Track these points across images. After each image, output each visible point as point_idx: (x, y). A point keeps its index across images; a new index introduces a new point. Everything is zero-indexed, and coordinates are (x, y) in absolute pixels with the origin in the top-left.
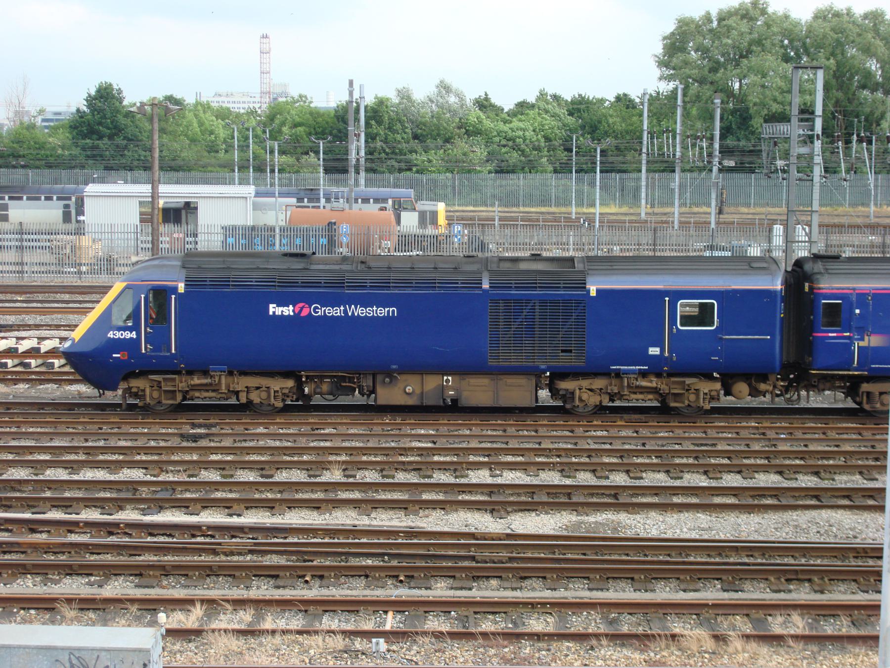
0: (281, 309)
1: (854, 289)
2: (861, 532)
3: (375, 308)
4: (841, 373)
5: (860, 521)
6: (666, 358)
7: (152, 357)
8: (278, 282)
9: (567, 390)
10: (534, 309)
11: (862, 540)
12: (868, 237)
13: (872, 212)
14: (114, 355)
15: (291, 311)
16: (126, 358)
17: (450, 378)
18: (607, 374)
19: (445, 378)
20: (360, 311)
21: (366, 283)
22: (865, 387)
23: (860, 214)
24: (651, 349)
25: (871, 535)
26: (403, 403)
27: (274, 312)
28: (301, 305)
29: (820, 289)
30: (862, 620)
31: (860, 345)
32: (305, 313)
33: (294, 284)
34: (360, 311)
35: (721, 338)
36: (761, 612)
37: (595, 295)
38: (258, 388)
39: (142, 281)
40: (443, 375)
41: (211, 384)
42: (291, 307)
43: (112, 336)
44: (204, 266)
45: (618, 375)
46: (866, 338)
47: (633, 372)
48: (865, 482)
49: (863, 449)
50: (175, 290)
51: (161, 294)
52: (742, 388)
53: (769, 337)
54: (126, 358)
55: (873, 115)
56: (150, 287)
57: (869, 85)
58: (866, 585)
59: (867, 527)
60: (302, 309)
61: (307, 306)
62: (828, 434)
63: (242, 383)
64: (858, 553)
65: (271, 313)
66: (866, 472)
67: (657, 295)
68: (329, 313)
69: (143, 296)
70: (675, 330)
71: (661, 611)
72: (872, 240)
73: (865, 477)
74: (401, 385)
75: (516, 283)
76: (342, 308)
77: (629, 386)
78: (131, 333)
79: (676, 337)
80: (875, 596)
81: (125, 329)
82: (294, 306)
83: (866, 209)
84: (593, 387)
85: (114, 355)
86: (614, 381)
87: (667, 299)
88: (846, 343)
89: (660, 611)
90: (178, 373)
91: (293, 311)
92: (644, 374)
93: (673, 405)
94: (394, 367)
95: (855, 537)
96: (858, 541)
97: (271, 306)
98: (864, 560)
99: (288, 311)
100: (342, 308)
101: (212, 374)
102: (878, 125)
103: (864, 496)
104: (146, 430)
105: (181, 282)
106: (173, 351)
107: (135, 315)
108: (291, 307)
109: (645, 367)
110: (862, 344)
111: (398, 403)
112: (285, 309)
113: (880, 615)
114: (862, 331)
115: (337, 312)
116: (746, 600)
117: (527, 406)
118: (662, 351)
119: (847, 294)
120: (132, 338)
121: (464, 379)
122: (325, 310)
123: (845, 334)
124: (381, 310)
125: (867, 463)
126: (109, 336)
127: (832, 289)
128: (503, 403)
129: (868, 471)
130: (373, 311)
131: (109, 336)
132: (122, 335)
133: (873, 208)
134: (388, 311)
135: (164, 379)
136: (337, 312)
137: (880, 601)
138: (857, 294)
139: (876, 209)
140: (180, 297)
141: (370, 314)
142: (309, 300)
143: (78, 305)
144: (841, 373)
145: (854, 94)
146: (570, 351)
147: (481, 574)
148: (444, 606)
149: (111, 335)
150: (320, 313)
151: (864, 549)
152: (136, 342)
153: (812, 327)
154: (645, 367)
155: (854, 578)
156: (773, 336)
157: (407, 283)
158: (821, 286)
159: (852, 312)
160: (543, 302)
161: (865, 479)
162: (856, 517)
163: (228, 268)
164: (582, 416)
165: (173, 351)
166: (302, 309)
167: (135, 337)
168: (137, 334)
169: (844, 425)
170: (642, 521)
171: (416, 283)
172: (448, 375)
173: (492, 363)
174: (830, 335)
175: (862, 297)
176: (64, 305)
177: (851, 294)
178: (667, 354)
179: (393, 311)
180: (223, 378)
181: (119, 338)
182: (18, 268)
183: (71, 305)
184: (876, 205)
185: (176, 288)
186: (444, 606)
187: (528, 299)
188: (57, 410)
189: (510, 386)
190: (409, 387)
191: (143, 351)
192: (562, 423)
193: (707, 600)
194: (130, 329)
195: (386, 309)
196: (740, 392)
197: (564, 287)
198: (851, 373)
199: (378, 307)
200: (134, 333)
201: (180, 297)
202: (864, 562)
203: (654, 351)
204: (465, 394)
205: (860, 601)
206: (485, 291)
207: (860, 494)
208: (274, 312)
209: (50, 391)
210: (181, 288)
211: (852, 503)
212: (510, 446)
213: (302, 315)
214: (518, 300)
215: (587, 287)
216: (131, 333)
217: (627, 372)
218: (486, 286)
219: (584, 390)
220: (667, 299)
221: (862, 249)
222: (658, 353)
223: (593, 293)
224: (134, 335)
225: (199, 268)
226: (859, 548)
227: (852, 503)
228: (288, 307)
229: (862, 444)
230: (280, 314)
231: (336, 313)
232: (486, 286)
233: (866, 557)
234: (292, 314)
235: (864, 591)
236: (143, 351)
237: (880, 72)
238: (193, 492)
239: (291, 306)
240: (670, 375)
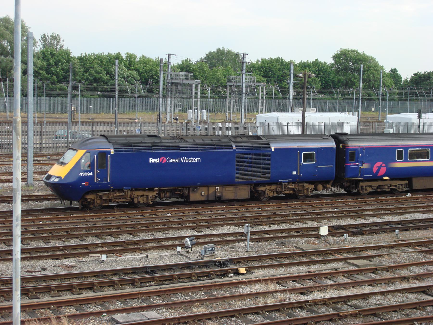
0: (154, 160)
2: (5, 272)
3: (192, 159)
5: (4, 266)
6: (298, 176)
9: (262, 191)
11: (6, 275)
12: (6, 127)
13: (8, 115)
14: (82, 184)
16: (87, 185)
18: (276, 183)
19: (217, 188)
20: (186, 160)
21: (122, 148)
22: (361, 184)
23: (2, 116)
24: (293, 172)
25: (10, 273)
26: (200, 200)
27: (151, 162)
28: (162, 158)
29: (348, 146)
30: (7, 315)
32: (164, 162)
33: (159, 149)
34: (186, 160)
35: (317, 167)
36: (31, 308)
38: (141, 196)
39: (94, 149)
40: (216, 187)
42: (158, 159)
43: (81, 175)
44: (118, 142)
45: (281, 183)
46: (363, 165)
48: (7, 247)
49: (5, 231)
50: (109, 153)
51: (103, 155)
52: (320, 186)
55: (7, 67)
56: (98, 152)
57: (4, 53)
58: (8, 297)
59: (8, 269)
60: (163, 159)
62: (35, 222)
64: (4, 282)
65: (150, 162)
66: (7, 242)
67: (295, 150)
69: (96, 156)
71: (31, 309)
72: (8, 129)
73: (7, 245)
76: (179, 159)
77: (285, 188)
78: (90, 173)
79: (302, 166)
80: (8, 303)
81: (87, 171)
82: (160, 159)
83: (5, 114)
84: (272, 189)
85: (82, 184)
86: (279, 186)
87: (299, 152)
89: (78, 303)
90: (109, 191)
91: (159, 161)
92: (289, 183)
94: (199, 184)
95: (2, 275)
96: (4, 276)
97: (150, 159)
98: (7, 285)
99: (157, 161)
100: (179, 159)
102: (10, 72)
103: (6, 254)
104: (41, 223)
105: (112, 149)
106: (109, 181)
107: (91, 166)
108: (158, 159)
110: (362, 167)
111: (198, 200)
112: (156, 160)
113: (12, 312)
114: (362, 163)
115: (177, 160)
116: (124, 293)
118: (297, 173)
120: (90, 176)
121: (224, 188)
125: (8, 238)
126: (80, 175)
128: (239, 197)
129: (8, 242)
131: (80, 175)
132: (86, 174)
133: (8, 113)
134: (197, 160)
135: (103, 194)
136: (177, 160)
137: (12, 305)
139: (10, 114)
140: (112, 155)
142: (166, 155)
146: (265, 174)
147: (82, 287)
148: (70, 303)
149: (81, 174)
151: (6, 280)
153: (345, 162)
155: (2, 295)
157: (203, 148)
158: (349, 145)
159: (359, 155)
160: (256, 154)
161: (7, 246)
162: (2, 265)
164: (95, 211)
165: (109, 181)
166: (163, 159)
167: (92, 175)
168: (93, 174)
169: (76, 215)
171: (208, 147)
172: (218, 186)
173: (236, 180)
174: (352, 164)
175: (362, 149)
178: (299, 174)
179: (199, 159)
180: (129, 192)
184: (10, 112)
186: (70, 303)
187: (250, 153)
188: (34, 213)
190: (203, 193)
191: (96, 181)
192: (285, 203)
194: (90, 171)
195: (197, 159)
199: (193, 158)
200: (92, 173)
201: (112, 155)
202: (7, 286)
203: (294, 173)
204: (224, 194)
205: (5, 305)
207: (4, 253)
208: (151, 162)
209: (45, 204)
210: (112, 151)
211: (89, 251)
212: (63, 228)
213: (163, 162)
214: (246, 153)
215: (271, 147)
216: (90, 173)
217: (284, 182)
218: (234, 147)
219: (268, 190)
221: (3, 133)
222: (296, 174)
223: (273, 150)
224: (91, 174)
225: (117, 142)
226: (4, 280)
227: (89, 251)
228: (191, 158)
229: (5, 229)
232: (234, 147)
233: (8, 284)
234: (159, 162)
235: (7, 301)
236: (96, 181)
237: (9, 47)
238: (234, 237)
239: (158, 159)
240: (299, 182)
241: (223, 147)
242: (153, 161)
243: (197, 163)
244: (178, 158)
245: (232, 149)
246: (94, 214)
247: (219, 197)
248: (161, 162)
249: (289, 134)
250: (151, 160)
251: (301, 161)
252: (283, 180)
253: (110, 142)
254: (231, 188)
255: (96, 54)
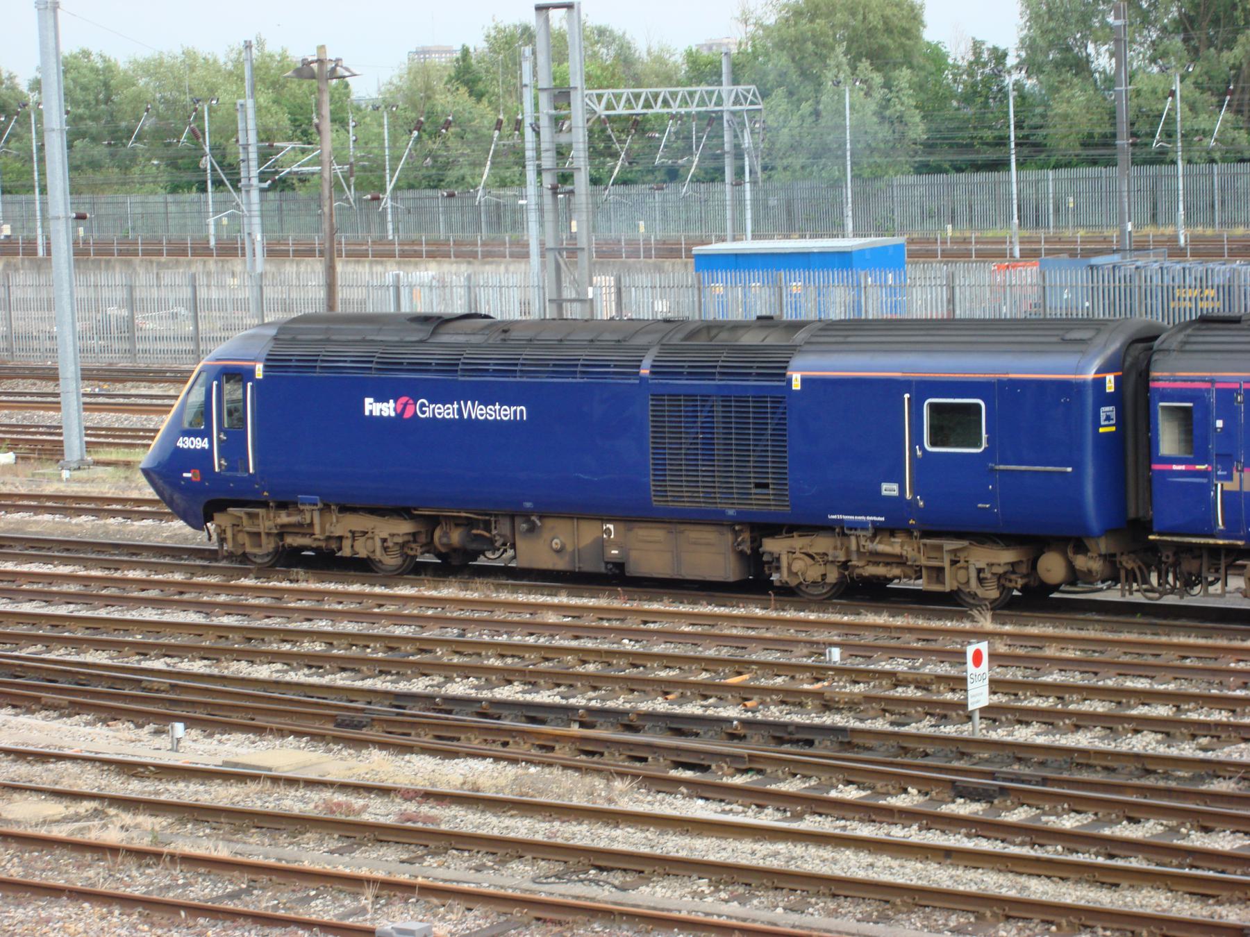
1: (1212, 381)
3: (497, 407)
4: (1194, 540)
6: (909, 503)
7: (228, 480)
8: (377, 363)
10: (713, 411)
15: (392, 409)
16: (198, 479)
17: (611, 527)
20: (478, 411)
21: (291, 360)
24: (885, 486)
27: (371, 412)
28: (404, 400)
31: (1225, 489)
32: (408, 414)
33: (396, 366)
34: (478, 411)
35: (993, 470)
37: (799, 388)
41: (300, 525)
44: (300, 337)
45: (842, 531)
46: (1236, 475)
47: (863, 526)
53: (1069, 469)
54: (198, 479)
60: (405, 405)
61: (411, 402)
63: (343, 525)
65: (367, 413)
67: (889, 389)
68: (440, 414)
70: (919, 453)
74: (546, 535)
75: (689, 367)
76: (456, 406)
78: (203, 440)
79: (924, 465)
82: (395, 402)
84: (811, 551)
88: (1202, 484)
90: (264, 504)
91: (395, 410)
92: (878, 530)
93: (1110, 582)
97: (368, 401)
99: (387, 409)
100: (456, 406)
101: (302, 507)
109: (834, 517)
110: (1231, 486)
115: (447, 411)
117: (667, 576)
119: (1200, 390)
120: (203, 449)
121: (630, 530)
122: (434, 409)
123: (1198, 467)
124: (505, 410)
127: (1175, 381)
128: (690, 572)
130: (495, 411)
134: (515, 412)
136: (447, 411)
138: (1217, 390)
141: (491, 415)
142: (413, 391)
143: (126, 401)
144: (1194, 540)
145: (604, 69)
146: (766, 486)
150: (427, 414)
152: (207, 454)
154: (834, 517)
156: (1079, 467)
163: (328, 340)
166: (405, 405)
167: (207, 446)
170: (437, 775)
172: (609, 521)
174: (1175, 467)
176: (39, 399)
177: (1208, 390)
179: (521, 411)
181: (189, 448)
182: (1008, 289)
183: (133, 400)
185: (252, 372)
189: (695, 543)
190: (556, 541)
193: (811, 929)
195: (513, 409)
196: (1049, 571)
197: (758, 374)
198: (1211, 541)
199: (501, 405)
201: (258, 385)
203: (889, 489)
204: (634, 555)
206: (643, 380)
208: (371, 412)
210: (259, 374)
215: (789, 373)
216: (203, 440)
217: (854, 527)
220: (907, 396)
222: (896, 493)
223: (796, 386)
225: (294, 339)
228: (494, 405)
230: (378, 414)
231: (448, 414)
234: (393, 414)
239: (391, 401)
241: (608, 366)
242: (376, 413)
243: (512, 424)
244: (453, 404)
245: (638, 373)
246: (1201, 641)
247: (620, 566)
248: (400, 415)
249: (959, 314)
250: (371, 407)
251: (917, 438)
252: (846, 517)
253: (1128, 349)
254: (656, 534)
255: (273, 47)
